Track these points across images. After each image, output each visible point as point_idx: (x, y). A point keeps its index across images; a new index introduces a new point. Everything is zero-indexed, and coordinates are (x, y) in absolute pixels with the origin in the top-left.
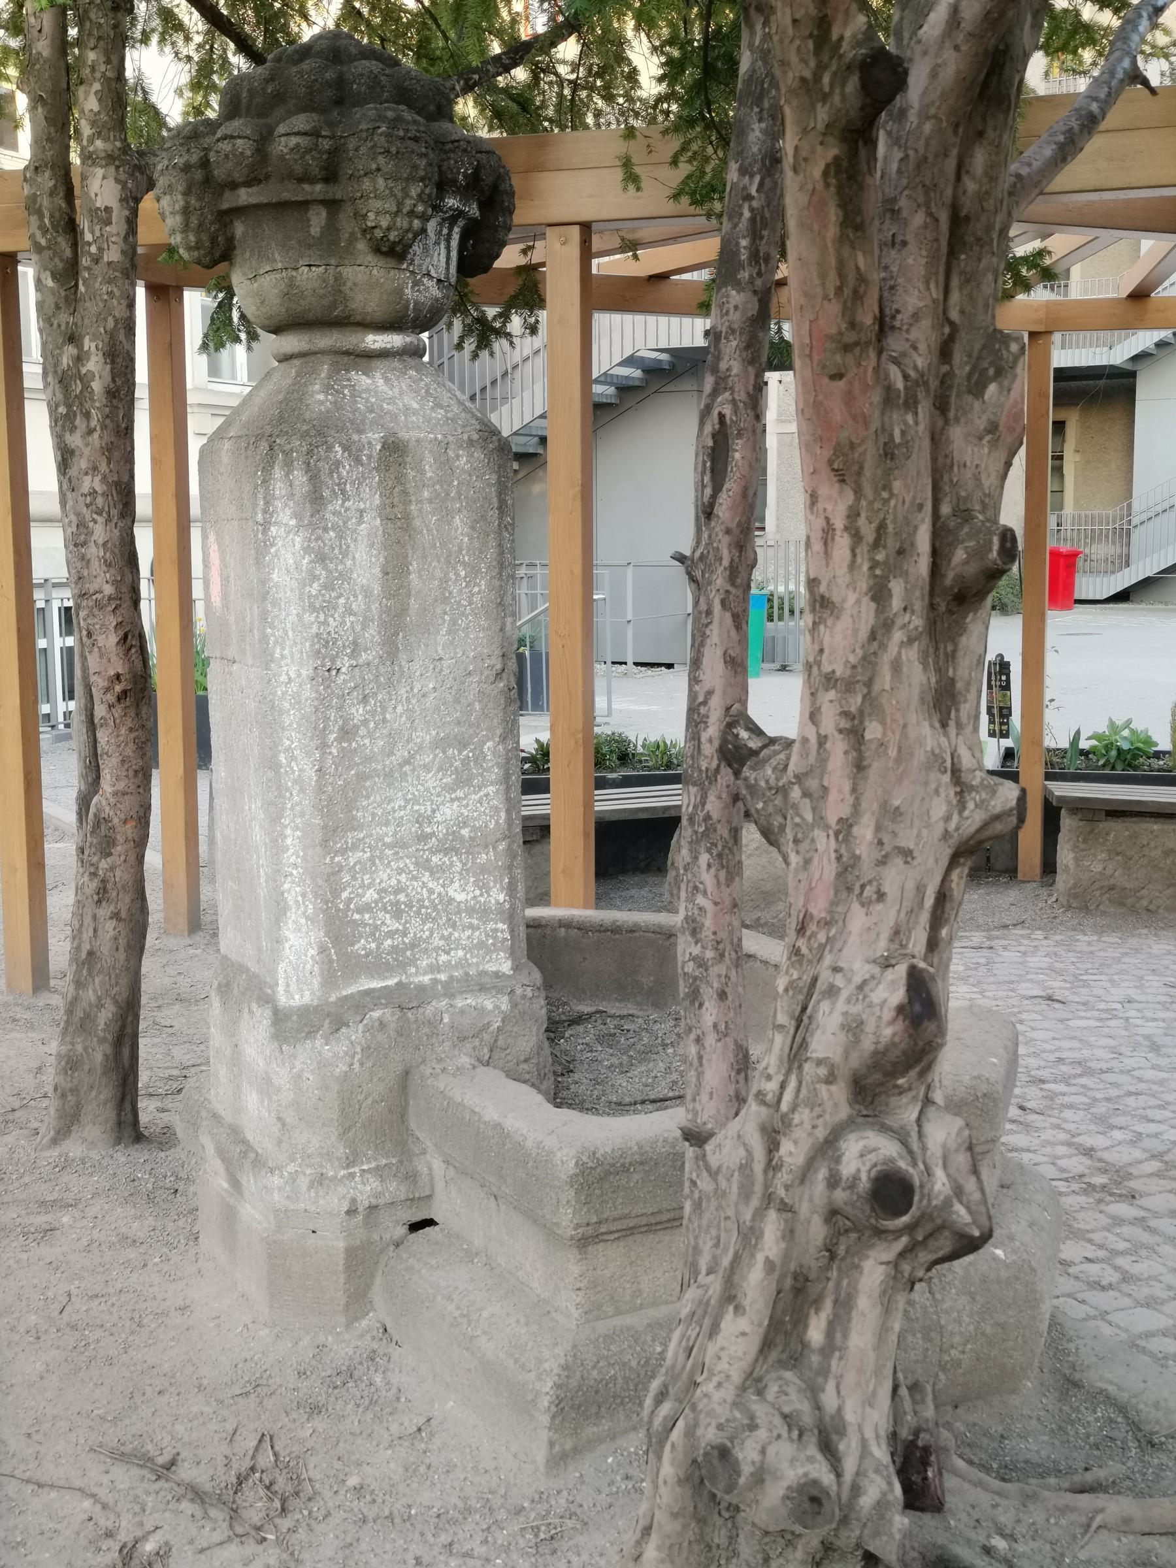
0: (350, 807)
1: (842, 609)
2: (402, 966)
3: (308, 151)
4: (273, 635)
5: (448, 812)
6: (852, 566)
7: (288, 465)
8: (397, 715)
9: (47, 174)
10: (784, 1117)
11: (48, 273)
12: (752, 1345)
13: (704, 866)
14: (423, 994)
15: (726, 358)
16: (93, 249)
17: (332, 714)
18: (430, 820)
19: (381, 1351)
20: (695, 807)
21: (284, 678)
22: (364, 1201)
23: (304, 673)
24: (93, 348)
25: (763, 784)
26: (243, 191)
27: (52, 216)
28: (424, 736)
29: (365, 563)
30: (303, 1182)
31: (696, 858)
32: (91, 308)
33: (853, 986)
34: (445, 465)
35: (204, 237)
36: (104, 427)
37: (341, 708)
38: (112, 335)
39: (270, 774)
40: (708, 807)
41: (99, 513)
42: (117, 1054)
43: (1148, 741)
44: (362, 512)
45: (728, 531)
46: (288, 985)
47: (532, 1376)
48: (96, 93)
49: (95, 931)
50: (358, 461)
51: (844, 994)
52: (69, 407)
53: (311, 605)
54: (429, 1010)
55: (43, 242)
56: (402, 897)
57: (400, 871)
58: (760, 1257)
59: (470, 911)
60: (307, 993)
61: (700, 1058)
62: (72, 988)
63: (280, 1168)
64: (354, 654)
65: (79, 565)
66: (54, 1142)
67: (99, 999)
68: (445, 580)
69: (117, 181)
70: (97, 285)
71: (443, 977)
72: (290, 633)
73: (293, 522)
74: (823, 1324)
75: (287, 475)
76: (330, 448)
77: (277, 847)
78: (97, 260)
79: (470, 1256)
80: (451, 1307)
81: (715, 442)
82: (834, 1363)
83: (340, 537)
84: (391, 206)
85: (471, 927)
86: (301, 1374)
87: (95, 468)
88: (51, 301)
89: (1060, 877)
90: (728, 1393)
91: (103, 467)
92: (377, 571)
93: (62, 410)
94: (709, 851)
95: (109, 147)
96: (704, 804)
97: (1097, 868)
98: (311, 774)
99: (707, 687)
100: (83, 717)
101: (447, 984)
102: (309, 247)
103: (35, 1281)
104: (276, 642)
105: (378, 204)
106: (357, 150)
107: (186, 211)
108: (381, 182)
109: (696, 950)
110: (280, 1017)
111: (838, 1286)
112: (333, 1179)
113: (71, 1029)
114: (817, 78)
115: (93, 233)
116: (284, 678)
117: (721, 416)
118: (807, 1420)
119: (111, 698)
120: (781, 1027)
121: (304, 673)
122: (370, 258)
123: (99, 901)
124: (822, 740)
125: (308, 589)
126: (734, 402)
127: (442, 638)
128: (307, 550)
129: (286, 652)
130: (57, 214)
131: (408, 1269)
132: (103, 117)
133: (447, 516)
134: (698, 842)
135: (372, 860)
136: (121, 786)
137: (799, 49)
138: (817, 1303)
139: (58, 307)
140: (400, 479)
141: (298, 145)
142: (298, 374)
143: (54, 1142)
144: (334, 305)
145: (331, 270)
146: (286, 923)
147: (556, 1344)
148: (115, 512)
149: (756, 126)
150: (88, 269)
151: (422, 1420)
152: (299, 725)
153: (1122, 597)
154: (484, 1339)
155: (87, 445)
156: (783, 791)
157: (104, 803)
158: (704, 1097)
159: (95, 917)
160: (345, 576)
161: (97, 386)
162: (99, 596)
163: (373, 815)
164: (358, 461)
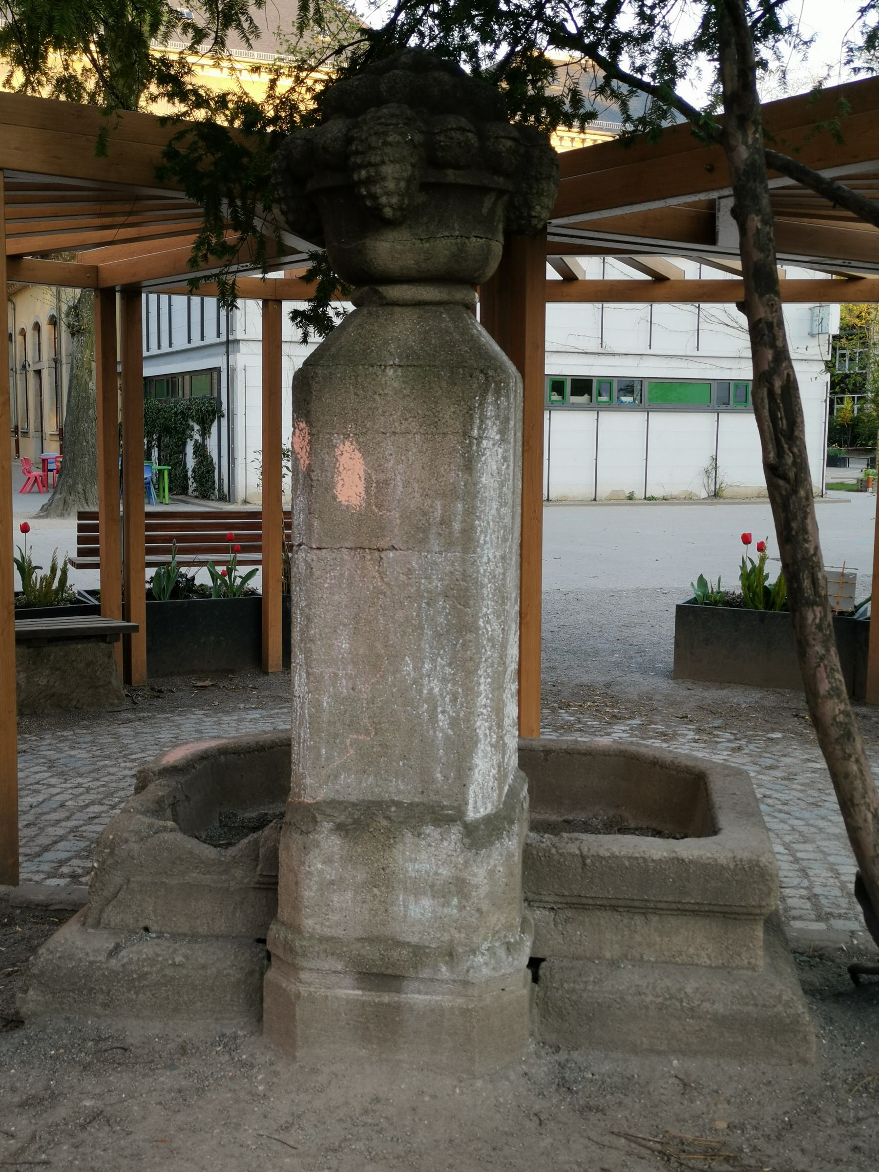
4: (480, 525)
20: (821, 619)
21: (485, 559)
30: (502, 953)
31: (828, 651)
46: (476, 802)
47: (780, 1008)
60: (489, 805)
61: (861, 771)
72: (491, 523)
73: (498, 437)
81: (782, 391)
97: (43, 682)
104: (481, 532)
110: (470, 830)
116: (485, 559)
129: (488, 539)
146: (477, 753)
152: (494, 595)
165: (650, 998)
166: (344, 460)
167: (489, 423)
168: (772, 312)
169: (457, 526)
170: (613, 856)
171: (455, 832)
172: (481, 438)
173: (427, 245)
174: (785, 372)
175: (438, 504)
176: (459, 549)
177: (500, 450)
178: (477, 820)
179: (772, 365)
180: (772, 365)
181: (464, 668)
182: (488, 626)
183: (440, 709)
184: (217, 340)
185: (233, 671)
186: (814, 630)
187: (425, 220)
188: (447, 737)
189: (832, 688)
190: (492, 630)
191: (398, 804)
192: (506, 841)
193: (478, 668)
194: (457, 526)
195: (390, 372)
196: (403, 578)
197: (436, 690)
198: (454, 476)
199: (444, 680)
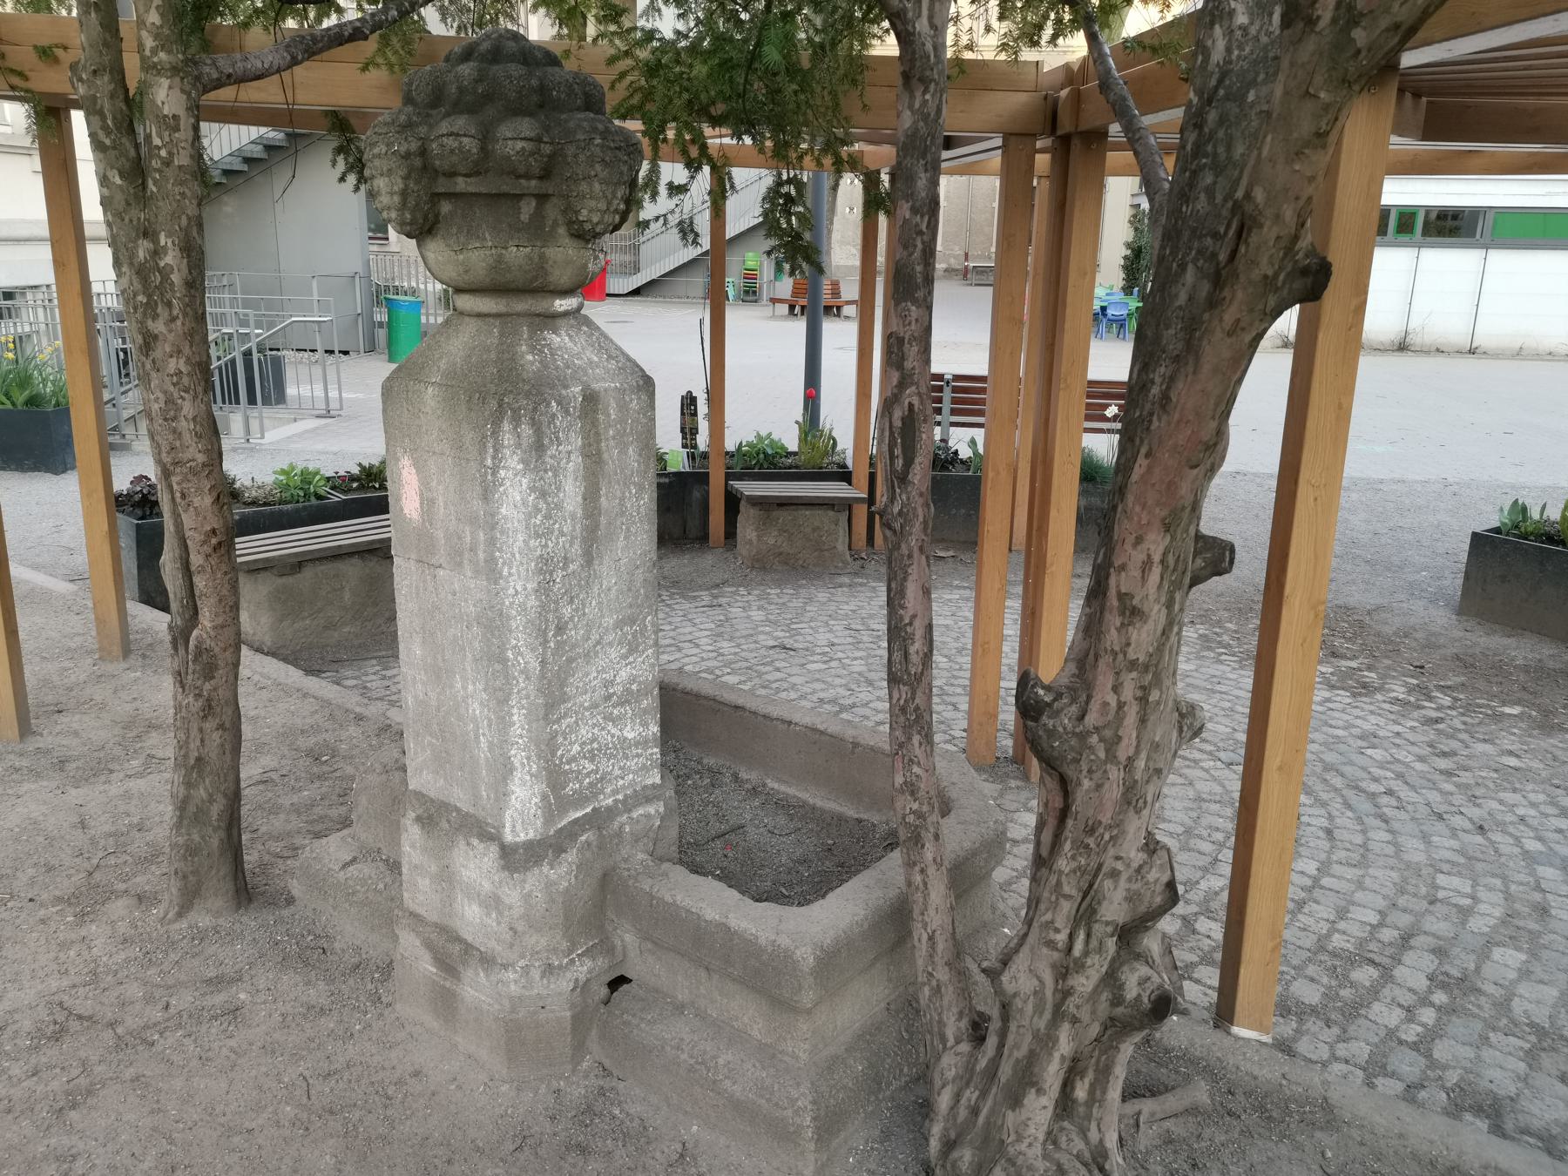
0: (563, 685)
1: (1148, 617)
2: (595, 795)
3: (532, 154)
5: (624, 674)
6: (1160, 587)
7: (516, 421)
8: (591, 610)
9: (106, 78)
10: (1076, 961)
12: (1049, 1113)
14: (611, 812)
16: (163, 153)
17: (550, 616)
18: (612, 683)
19: (606, 1086)
21: (511, 591)
22: (582, 978)
23: (529, 586)
26: (460, 180)
27: (114, 118)
28: (609, 621)
29: (571, 494)
30: (536, 974)
31: (910, 739)
32: (165, 208)
33: (1131, 870)
34: (623, 407)
35: (419, 216)
36: (185, 315)
37: (556, 610)
38: (187, 232)
39: (498, 667)
40: (917, 701)
41: (186, 391)
42: (229, 836)
43: (783, 447)
44: (569, 453)
45: (921, 495)
47: (789, 1112)
48: (157, 7)
49: (202, 741)
50: (567, 412)
51: (1124, 877)
52: (149, 296)
53: (536, 533)
54: (616, 825)
55: (108, 142)
56: (595, 745)
57: (594, 726)
58: (1057, 1055)
59: (637, 744)
61: (925, 884)
62: (182, 789)
63: (513, 965)
65: (171, 437)
66: (180, 915)
67: (211, 795)
68: (622, 499)
69: (183, 91)
71: (620, 797)
73: (520, 467)
74: (1087, 1086)
75: (515, 428)
76: (548, 405)
77: (504, 723)
78: (167, 163)
79: (680, 1008)
80: (684, 1056)
82: (1095, 1111)
83: (555, 476)
84: (602, 205)
85: (638, 756)
86: (553, 1118)
87: (179, 352)
88: (119, 198)
89: (742, 548)
90: (1037, 1150)
91: (187, 350)
92: (579, 499)
93: (141, 298)
94: (919, 733)
95: (172, 58)
98: (535, 665)
99: (911, 613)
101: (624, 801)
102: (519, 230)
103: (264, 1069)
105: (593, 203)
106: (575, 156)
107: (404, 194)
108: (597, 186)
109: (915, 806)
111: (1098, 1061)
112: (560, 967)
113: (185, 822)
114: (1276, 275)
116: (511, 591)
117: (911, 405)
118: (1087, 1155)
120: (1068, 897)
121: (529, 586)
122: (567, 240)
123: (205, 717)
124: (1121, 705)
126: (919, 394)
127: (621, 543)
128: (532, 489)
131: (624, 1023)
132: (166, 31)
134: (910, 727)
135: (576, 722)
136: (220, 620)
137: (1271, 256)
138: (1082, 1075)
139: (128, 204)
140: (595, 423)
142: (502, 335)
143: (180, 915)
144: (536, 278)
145: (536, 250)
147: (798, 1084)
148: (200, 389)
150: (160, 171)
151: (679, 1147)
153: (636, 292)
154: (728, 1083)
156: (1083, 736)
158: (931, 912)
159: (201, 730)
160: (559, 507)
161: (175, 278)
164: (567, 412)
165: (684, 1056)
166: (405, 473)
167: (507, 452)
169: (481, 556)
170: (674, 904)
171: (494, 849)
178: (516, 844)
187: (455, 230)
188: (487, 759)
189: (905, 783)
191: (458, 810)
192: (545, 869)
194: (481, 556)
195: (430, 390)
196: (450, 597)
199: (481, 704)
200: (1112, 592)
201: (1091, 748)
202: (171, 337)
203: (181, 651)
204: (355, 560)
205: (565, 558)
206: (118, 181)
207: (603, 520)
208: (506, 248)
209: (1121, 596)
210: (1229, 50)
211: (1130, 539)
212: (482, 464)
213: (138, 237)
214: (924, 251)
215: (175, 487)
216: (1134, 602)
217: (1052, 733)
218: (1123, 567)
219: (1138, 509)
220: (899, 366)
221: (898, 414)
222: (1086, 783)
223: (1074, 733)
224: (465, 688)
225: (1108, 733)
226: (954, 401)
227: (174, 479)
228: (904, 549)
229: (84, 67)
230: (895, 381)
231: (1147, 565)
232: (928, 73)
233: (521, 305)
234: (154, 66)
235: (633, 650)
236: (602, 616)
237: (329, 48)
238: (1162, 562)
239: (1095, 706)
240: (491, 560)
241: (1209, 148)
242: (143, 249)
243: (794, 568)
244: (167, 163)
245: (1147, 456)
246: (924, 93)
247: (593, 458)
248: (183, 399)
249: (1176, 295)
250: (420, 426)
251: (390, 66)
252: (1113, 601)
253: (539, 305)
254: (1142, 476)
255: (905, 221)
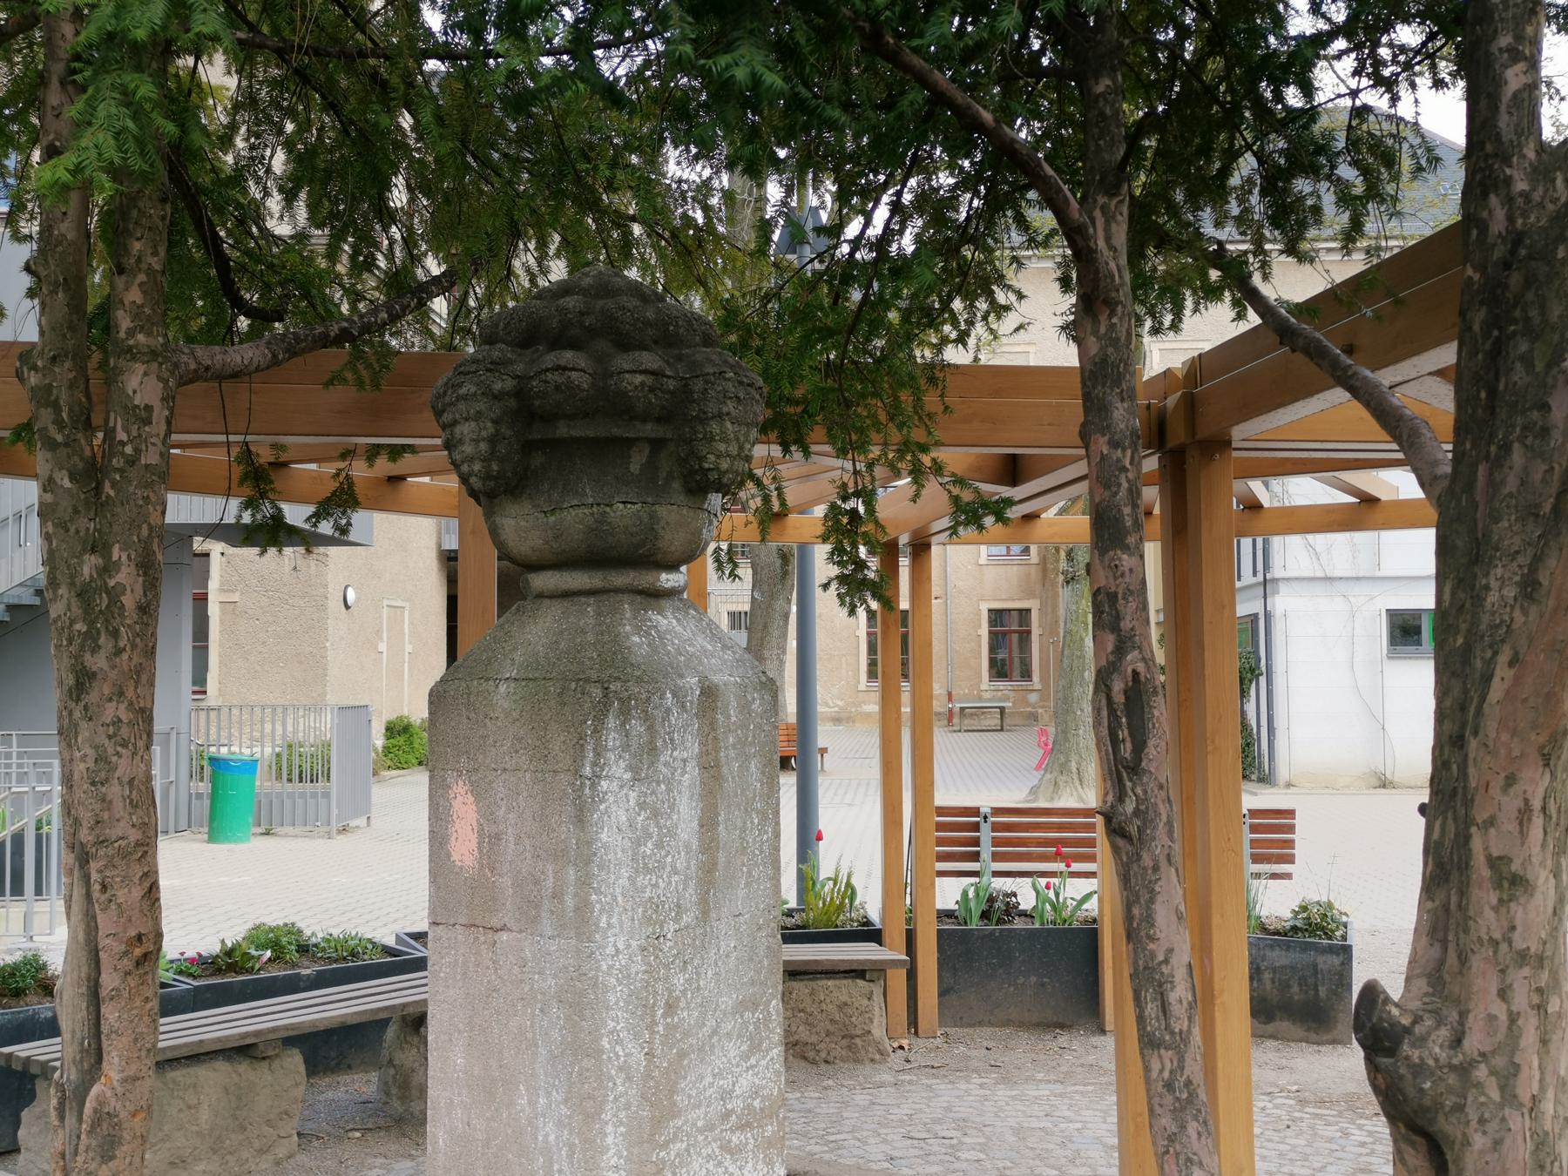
0: (672, 1091)
1: (1534, 888)
5: (745, 1083)
6: (1544, 845)
7: (625, 714)
11: (65, 472)
13: (1194, 1136)
15: (1128, 618)
16: (128, 450)
17: (660, 987)
21: (610, 950)
23: (634, 943)
24: (124, 558)
25: (1431, 1062)
28: (727, 1002)
29: (686, 814)
31: (1183, 1127)
34: (745, 707)
36: (134, 646)
37: (667, 979)
40: (1187, 1072)
41: (125, 745)
44: (685, 761)
48: (141, 285)
50: (683, 706)
55: (59, 438)
64: (677, 920)
65: (97, 807)
69: (159, 378)
70: (131, 489)
72: (620, 899)
73: (628, 776)
75: (623, 724)
78: (132, 462)
81: (1127, 698)
83: (669, 790)
87: (121, 694)
94: (1196, 1118)
96: (1182, 1069)
100: (84, 990)
104: (602, 911)
105: (722, 447)
107: (493, 441)
115: (127, 430)
116: (610, 950)
117: (1135, 673)
119: (127, 963)
121: (634, 943)
124: (1513, 1018)
125: (642, 849)
127: (741, 893)
128: (642, 806)
129: (614, 920)
130: (77, 409)
133: (745, 759)
134: (1183, 1109)
135: (687, 1150)
139: (76, 511)
140: (713, 725)
141: (643, 384)
142: (599, 614)
149: (1119, 405)
155: (114, 667)
156: (1464, 1070)
157: (109, 1094)
160: (672, 833)
162: (123, 843)
163: (690, 1097)
166: (457, 804)
168: (1116, 578)
169: (569, 902)
172: (599, 777)
173: (552, 519)
174: (1129, 670)
175: (550, 869)
176: (572, 934)
177: (633, 795)
179: (1111, 658)
180: (1111, 658)
181: (586, 1110)
182: (618, 1048)
183: (556, 1167)
184: (1253, 580)
185: (1062, 1026)
186: (1160, 1089)
187: (546, 486)
190: (626, 1055)
193: (600, 1109)
194: (569, 902)
195: (503, 688)
196: (516, 970)
197: (552, 1138)
198: (567, 832)
199: (560, 1124)
200: (1479, 860)
201: (1479, 1085)
202: (113, 674)
203: (70, 1120)
204: (221, 1065)
205: (679, 906)
206: (67, 483)
207: (722, 858)
208: (610, 505)
209: (1494, 863)
210: (1510, 219)
211: (1497, 783)
212: (577, 774)
213: (84, 551)
214: (1130, 490)
215: (95, 876)
216: (1514, 868)
217: (1419, 1070)
218: (1491, 822)
219: (1504, 737)
220: (1115, 628)
221: (1118, 686)
222: (1479, 1141)
223: (1452, 1067)
224: (532, 1103)
225: (1499, 1062)
226: (996, 842)
227: (94, 866)
228: (1147, 860)
229: (42, 353)
230: (1110, 648)
231: (1524, 814)
232: (1113, 294)
233: (620, 579)
234: (130, 349)
235: (755, 1048)
236: (720, 994)
237: (311, 350)
238: (1544, 809)
239: (1475, 1024)
240: (583, 907)
241: (1517, 313)
242: (89, 566)
243: (814, 1062)
244: (132, 462)
245: (1511, 664)
246: (1110, 317)
247: (710, 768)
248: (118, 754)
249: (1503, 482)
250: (484, 737)
251: (360, 384)
252: (1481, 869)
253: (643, 579)
254: (1508, 692)
255: (1103, 457)
